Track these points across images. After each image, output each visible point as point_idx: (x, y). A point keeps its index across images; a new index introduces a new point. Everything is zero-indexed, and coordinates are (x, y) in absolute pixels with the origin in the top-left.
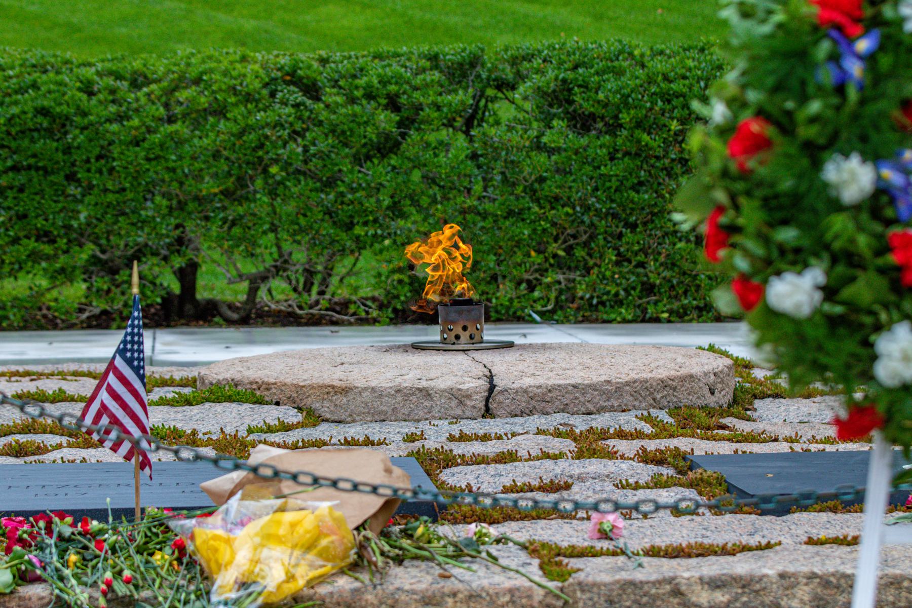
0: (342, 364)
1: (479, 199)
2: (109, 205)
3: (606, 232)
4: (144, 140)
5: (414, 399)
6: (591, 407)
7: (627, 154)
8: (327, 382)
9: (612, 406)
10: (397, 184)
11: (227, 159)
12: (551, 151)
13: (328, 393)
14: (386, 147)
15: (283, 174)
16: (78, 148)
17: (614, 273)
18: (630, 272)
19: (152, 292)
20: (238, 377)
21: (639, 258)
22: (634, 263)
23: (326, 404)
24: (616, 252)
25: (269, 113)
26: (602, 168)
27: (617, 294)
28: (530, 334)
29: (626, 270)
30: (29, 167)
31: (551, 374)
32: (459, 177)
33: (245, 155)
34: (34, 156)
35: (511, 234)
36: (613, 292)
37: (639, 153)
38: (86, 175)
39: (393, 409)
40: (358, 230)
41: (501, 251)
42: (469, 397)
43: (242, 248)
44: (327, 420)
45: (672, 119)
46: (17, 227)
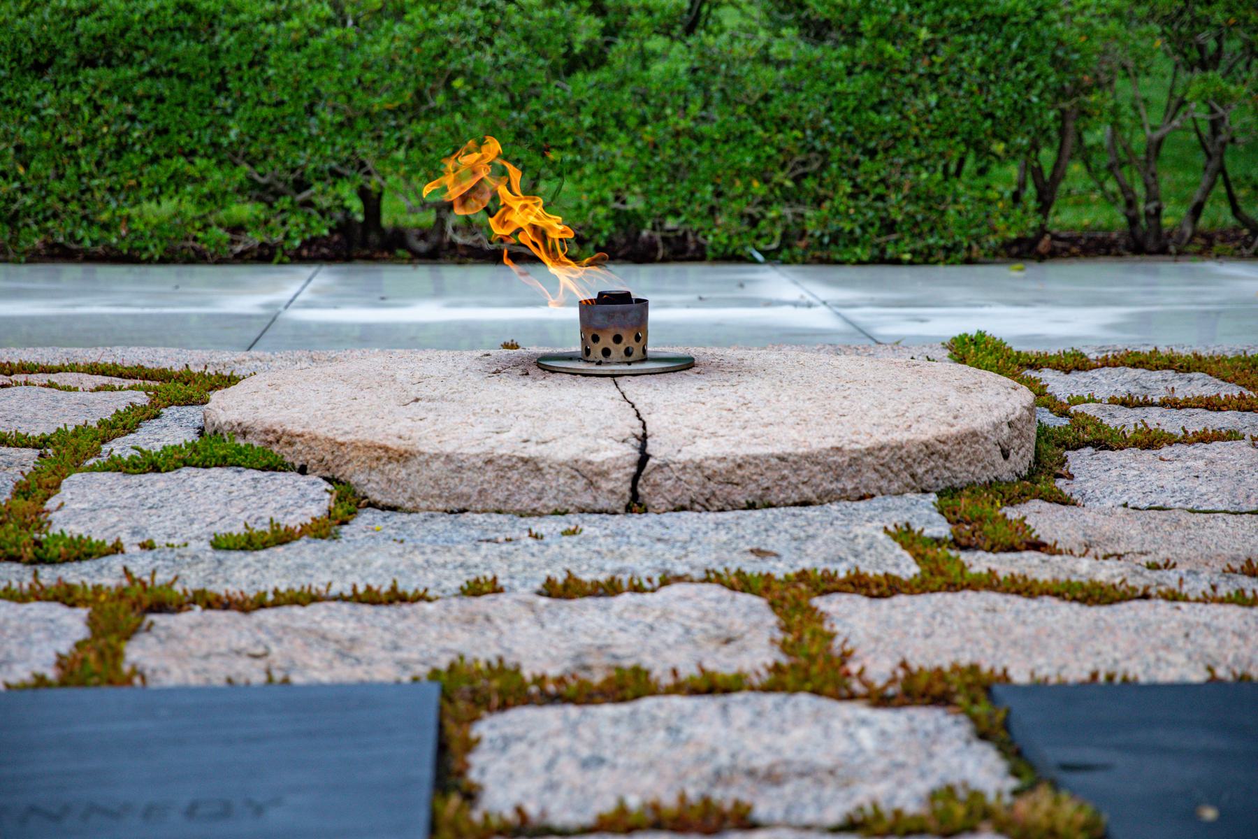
1: (694, 119)
2: (265, 120)
4: (306, 44)
5: (514, 475)
6: (808, 492)
7: (868, 67)
8: (379, 439)
9: (844, 490)
11: (403, 69)
12: (779, 65)
13: (378, 459)
14: (593, 58)
15: (469, 88)
16: (228, 50)
18: (868, 206)
20: (248, 420)
23: (375, 476)
25: (453, 16)
27: (852, 232)
28: (751, 281)
29: (862, 204)
30: (170, 74)
31: (743, 434)
34: (175, 60)
37: (882, 66)
39: (480, 492)
40: (553, 155)
42: (604, 474)
43: (421, 173)
44: (373, 505)
45: (921, 25)
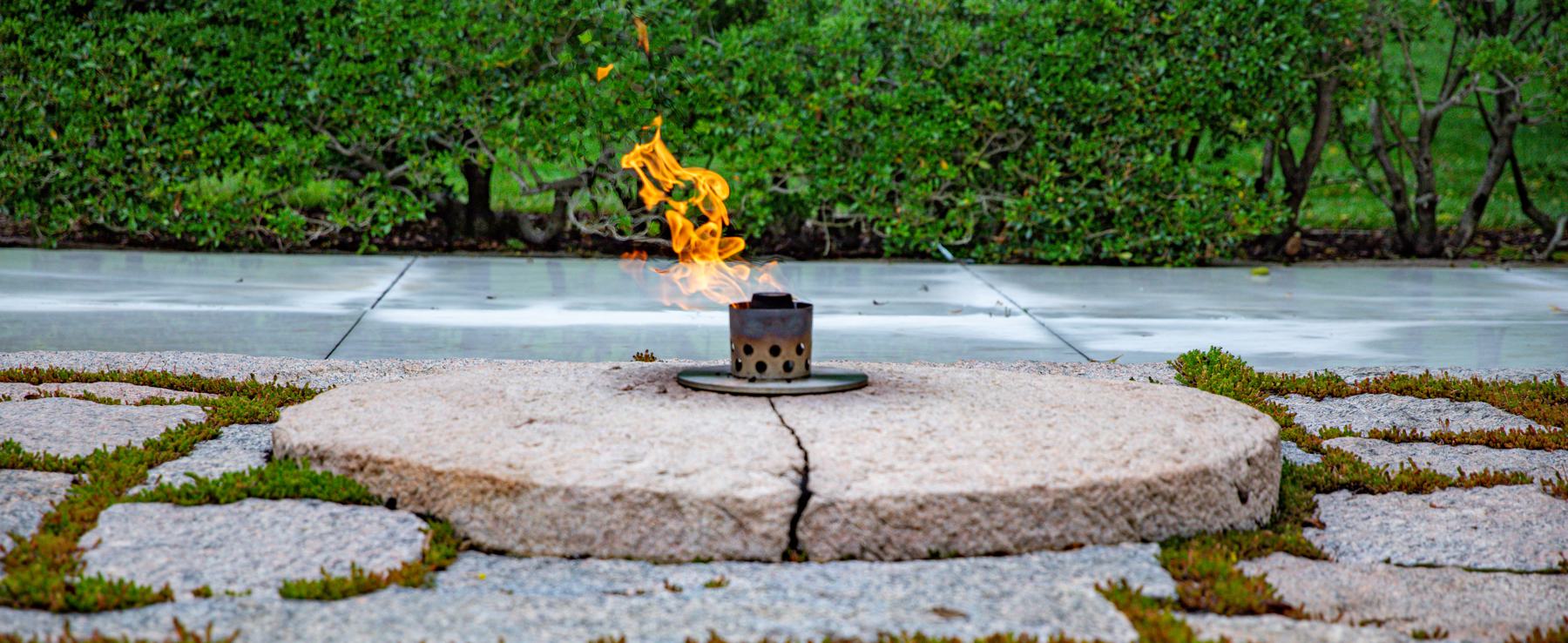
0: (531, 421)
1: (872, 86)
2: (350, 79)
3: (1048, 137)
5: (648, 514)
6: (1003, 540)
7: (1083, 25)
9: (1047, 538)
10: (758, 63)
13: (483, 492)
15: (598, 44)
17: (1057, 195)
18: (1079, 194)
19: (414, 204)
21: (1092, 175)
22: (1085, 182)
23: (479, 513)
24: (1060, 166)
26: (1046, 45)
27: (1060, 225)
29: (1074, 191)
30: (236, 21)
32: (844, 55)
33: (544, 15)
35: (915, 137)
36: (1054, 222)
38: (317, 34)
40: (702, 127)
41: (900, 161)
42: (756, 515)
43: (539, 146)
44: (476, 548)
46: (217, 106)
